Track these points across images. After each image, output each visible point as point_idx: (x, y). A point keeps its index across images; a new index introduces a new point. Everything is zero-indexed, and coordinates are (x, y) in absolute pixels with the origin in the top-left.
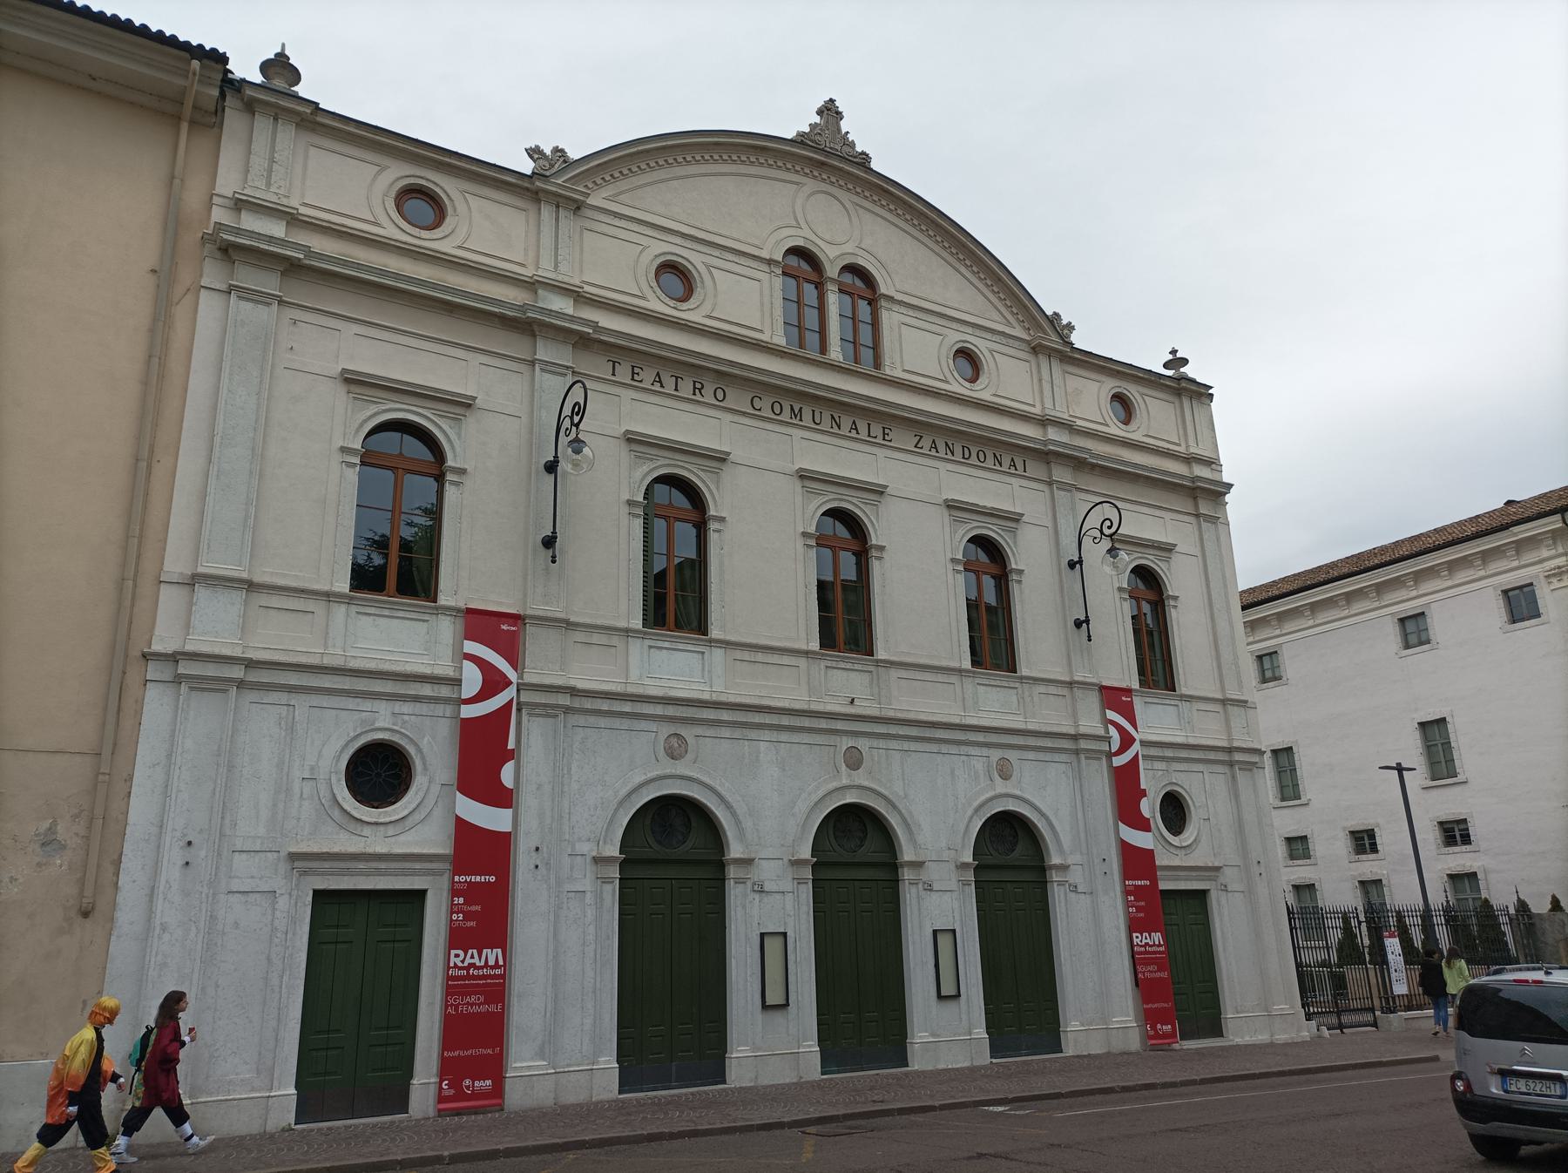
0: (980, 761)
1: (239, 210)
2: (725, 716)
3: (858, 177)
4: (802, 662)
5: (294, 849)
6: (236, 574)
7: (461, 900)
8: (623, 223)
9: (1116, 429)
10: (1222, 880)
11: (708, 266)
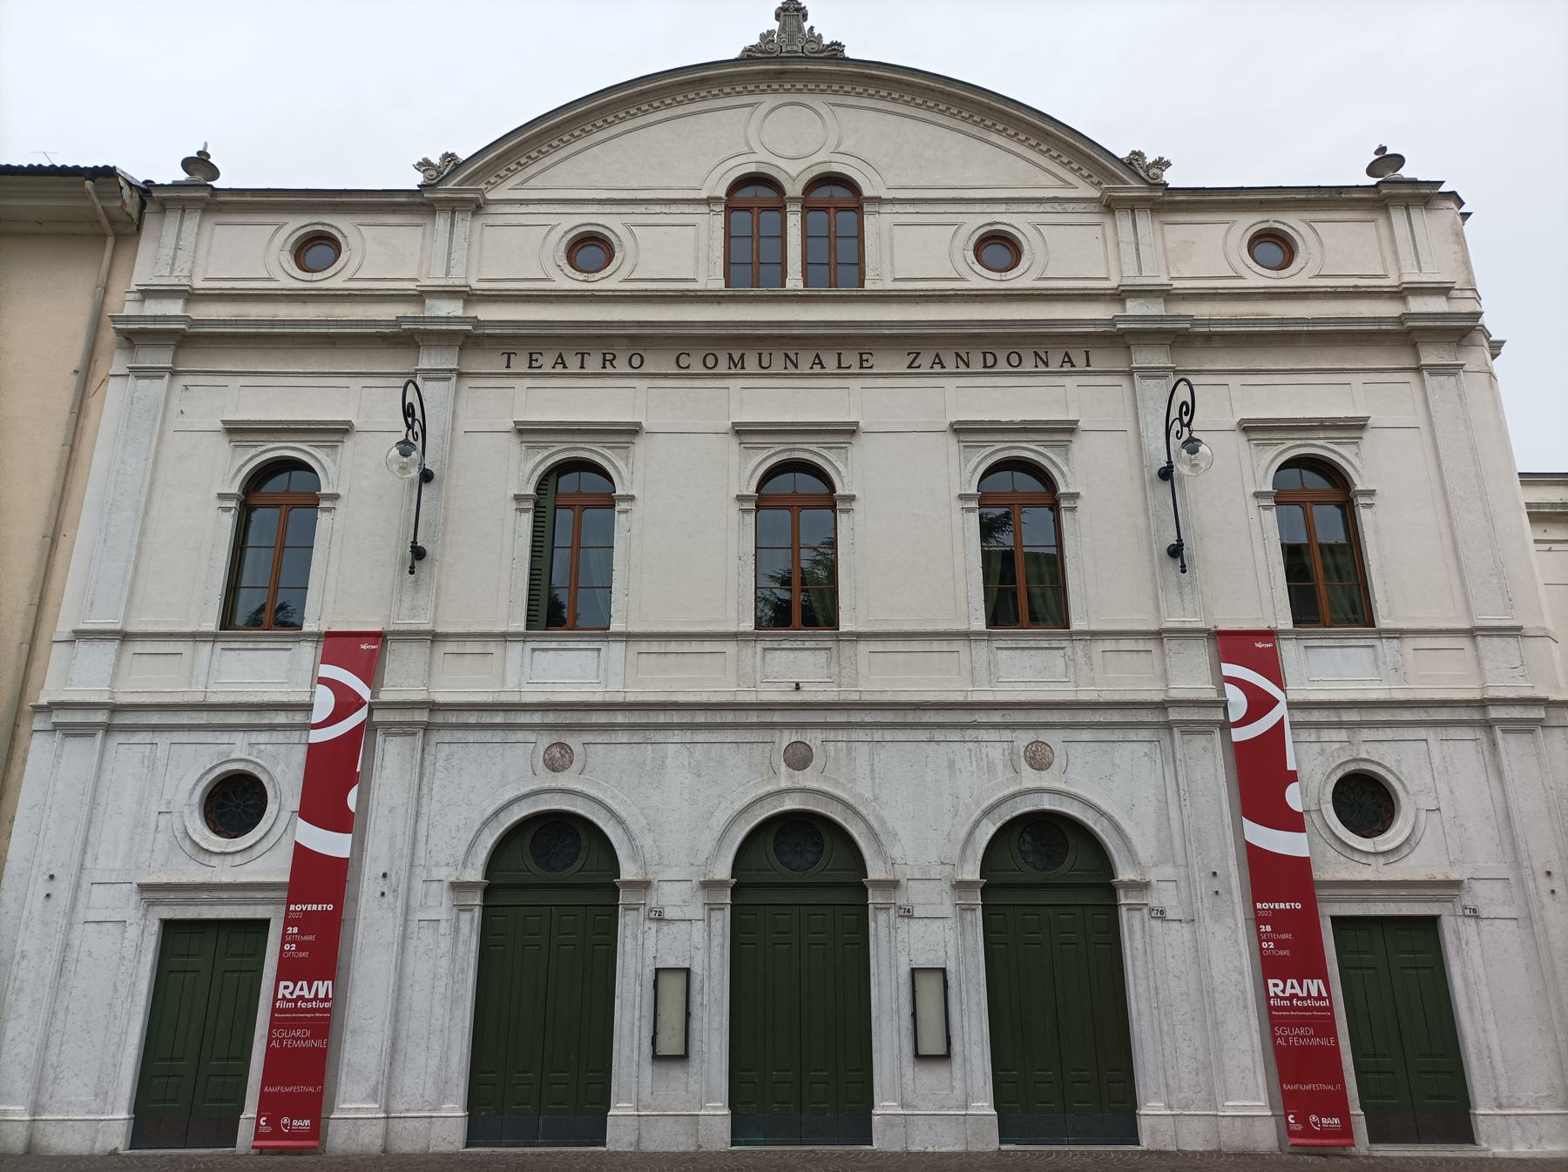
0: (996, 748)
2: (620, 718)
3: (830, 73)
4: (730, 648)
5: (144, 881)
6: (111, 627)
7: (296, 930)
8: (531, 208)
10: (1468, 900)
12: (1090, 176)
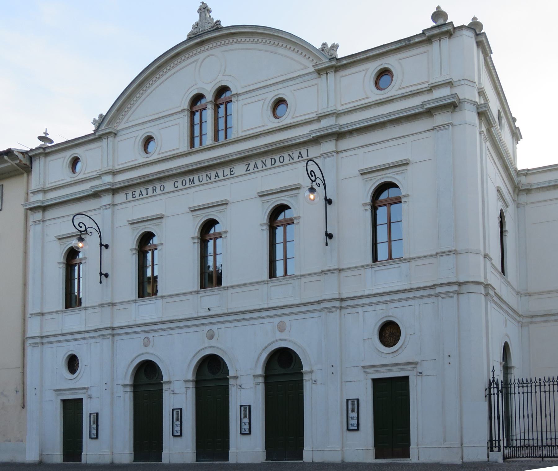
4: (190, 297)
11: (65, 157)
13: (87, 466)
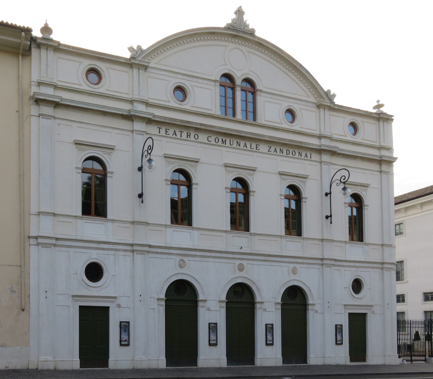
1: (39, 86)
4: (224, 234)
9: (350, 138)
11: (192, 86)
12: (314, 95)
13: (114, 371)
